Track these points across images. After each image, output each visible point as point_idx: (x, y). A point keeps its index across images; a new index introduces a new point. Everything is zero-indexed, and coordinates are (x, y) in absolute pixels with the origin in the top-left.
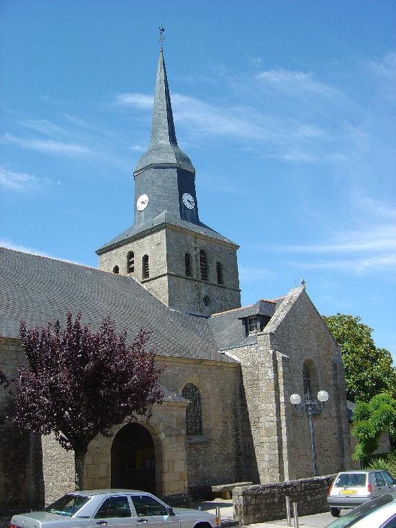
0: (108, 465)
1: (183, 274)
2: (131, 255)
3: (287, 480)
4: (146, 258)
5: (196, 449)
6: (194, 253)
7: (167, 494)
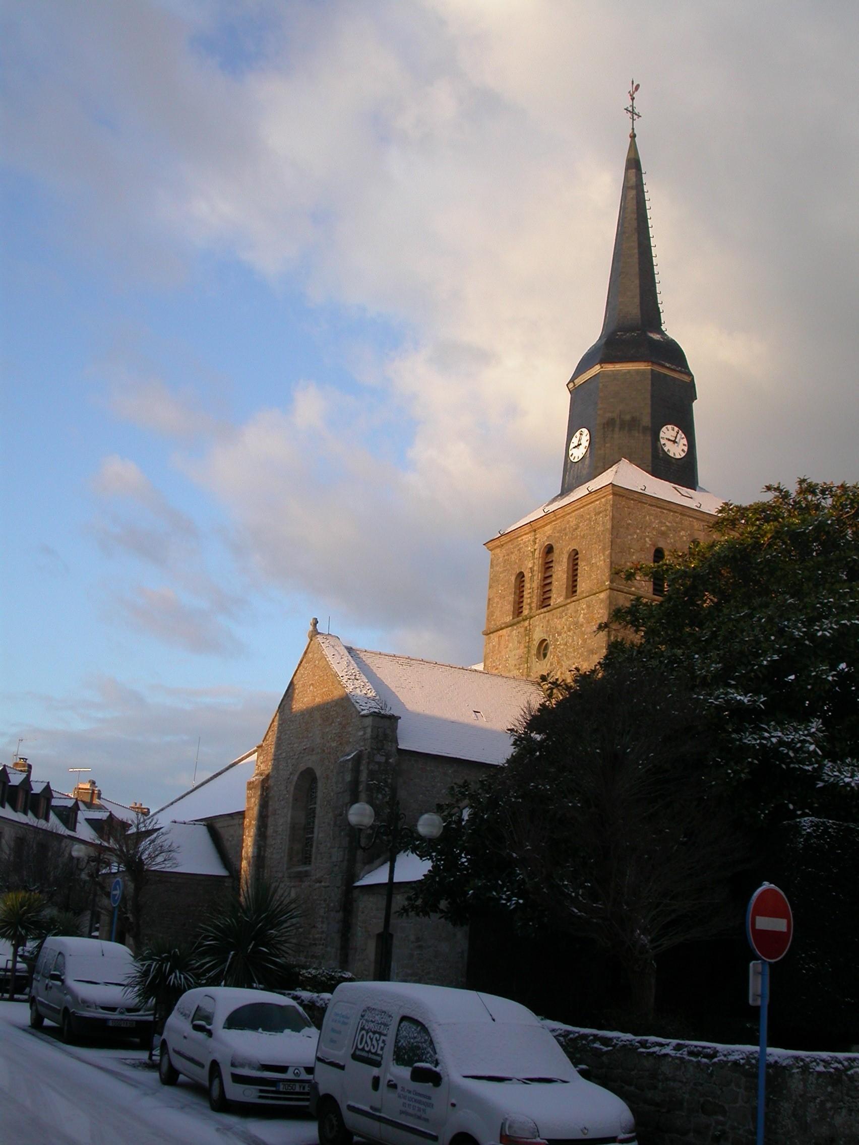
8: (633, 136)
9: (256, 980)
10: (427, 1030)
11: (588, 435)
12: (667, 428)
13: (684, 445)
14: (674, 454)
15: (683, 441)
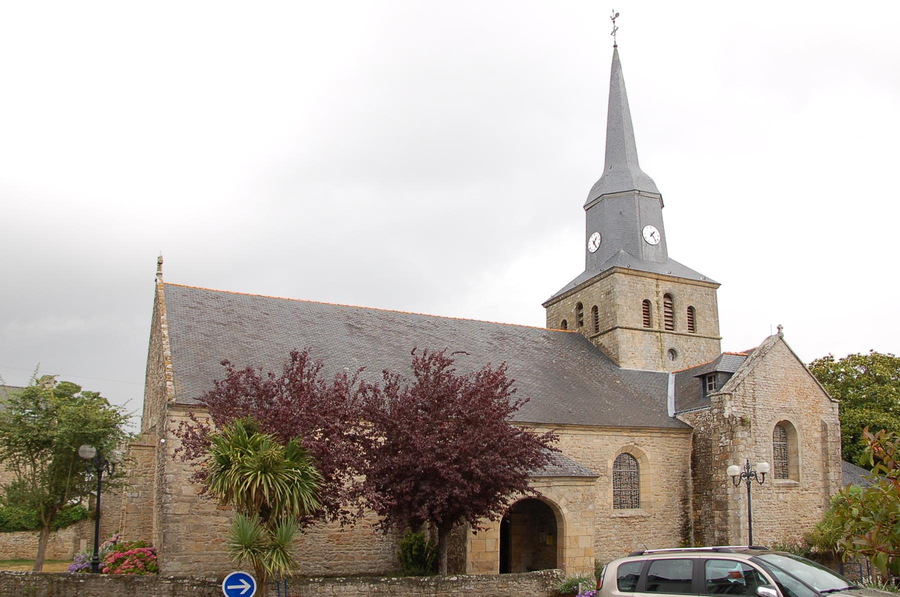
0: (497, 539)
1: (641, 326)
2: (580, 306)
4: (595, 309)
6: (655, 298)
7: (250, 586)
15: (657, 235)
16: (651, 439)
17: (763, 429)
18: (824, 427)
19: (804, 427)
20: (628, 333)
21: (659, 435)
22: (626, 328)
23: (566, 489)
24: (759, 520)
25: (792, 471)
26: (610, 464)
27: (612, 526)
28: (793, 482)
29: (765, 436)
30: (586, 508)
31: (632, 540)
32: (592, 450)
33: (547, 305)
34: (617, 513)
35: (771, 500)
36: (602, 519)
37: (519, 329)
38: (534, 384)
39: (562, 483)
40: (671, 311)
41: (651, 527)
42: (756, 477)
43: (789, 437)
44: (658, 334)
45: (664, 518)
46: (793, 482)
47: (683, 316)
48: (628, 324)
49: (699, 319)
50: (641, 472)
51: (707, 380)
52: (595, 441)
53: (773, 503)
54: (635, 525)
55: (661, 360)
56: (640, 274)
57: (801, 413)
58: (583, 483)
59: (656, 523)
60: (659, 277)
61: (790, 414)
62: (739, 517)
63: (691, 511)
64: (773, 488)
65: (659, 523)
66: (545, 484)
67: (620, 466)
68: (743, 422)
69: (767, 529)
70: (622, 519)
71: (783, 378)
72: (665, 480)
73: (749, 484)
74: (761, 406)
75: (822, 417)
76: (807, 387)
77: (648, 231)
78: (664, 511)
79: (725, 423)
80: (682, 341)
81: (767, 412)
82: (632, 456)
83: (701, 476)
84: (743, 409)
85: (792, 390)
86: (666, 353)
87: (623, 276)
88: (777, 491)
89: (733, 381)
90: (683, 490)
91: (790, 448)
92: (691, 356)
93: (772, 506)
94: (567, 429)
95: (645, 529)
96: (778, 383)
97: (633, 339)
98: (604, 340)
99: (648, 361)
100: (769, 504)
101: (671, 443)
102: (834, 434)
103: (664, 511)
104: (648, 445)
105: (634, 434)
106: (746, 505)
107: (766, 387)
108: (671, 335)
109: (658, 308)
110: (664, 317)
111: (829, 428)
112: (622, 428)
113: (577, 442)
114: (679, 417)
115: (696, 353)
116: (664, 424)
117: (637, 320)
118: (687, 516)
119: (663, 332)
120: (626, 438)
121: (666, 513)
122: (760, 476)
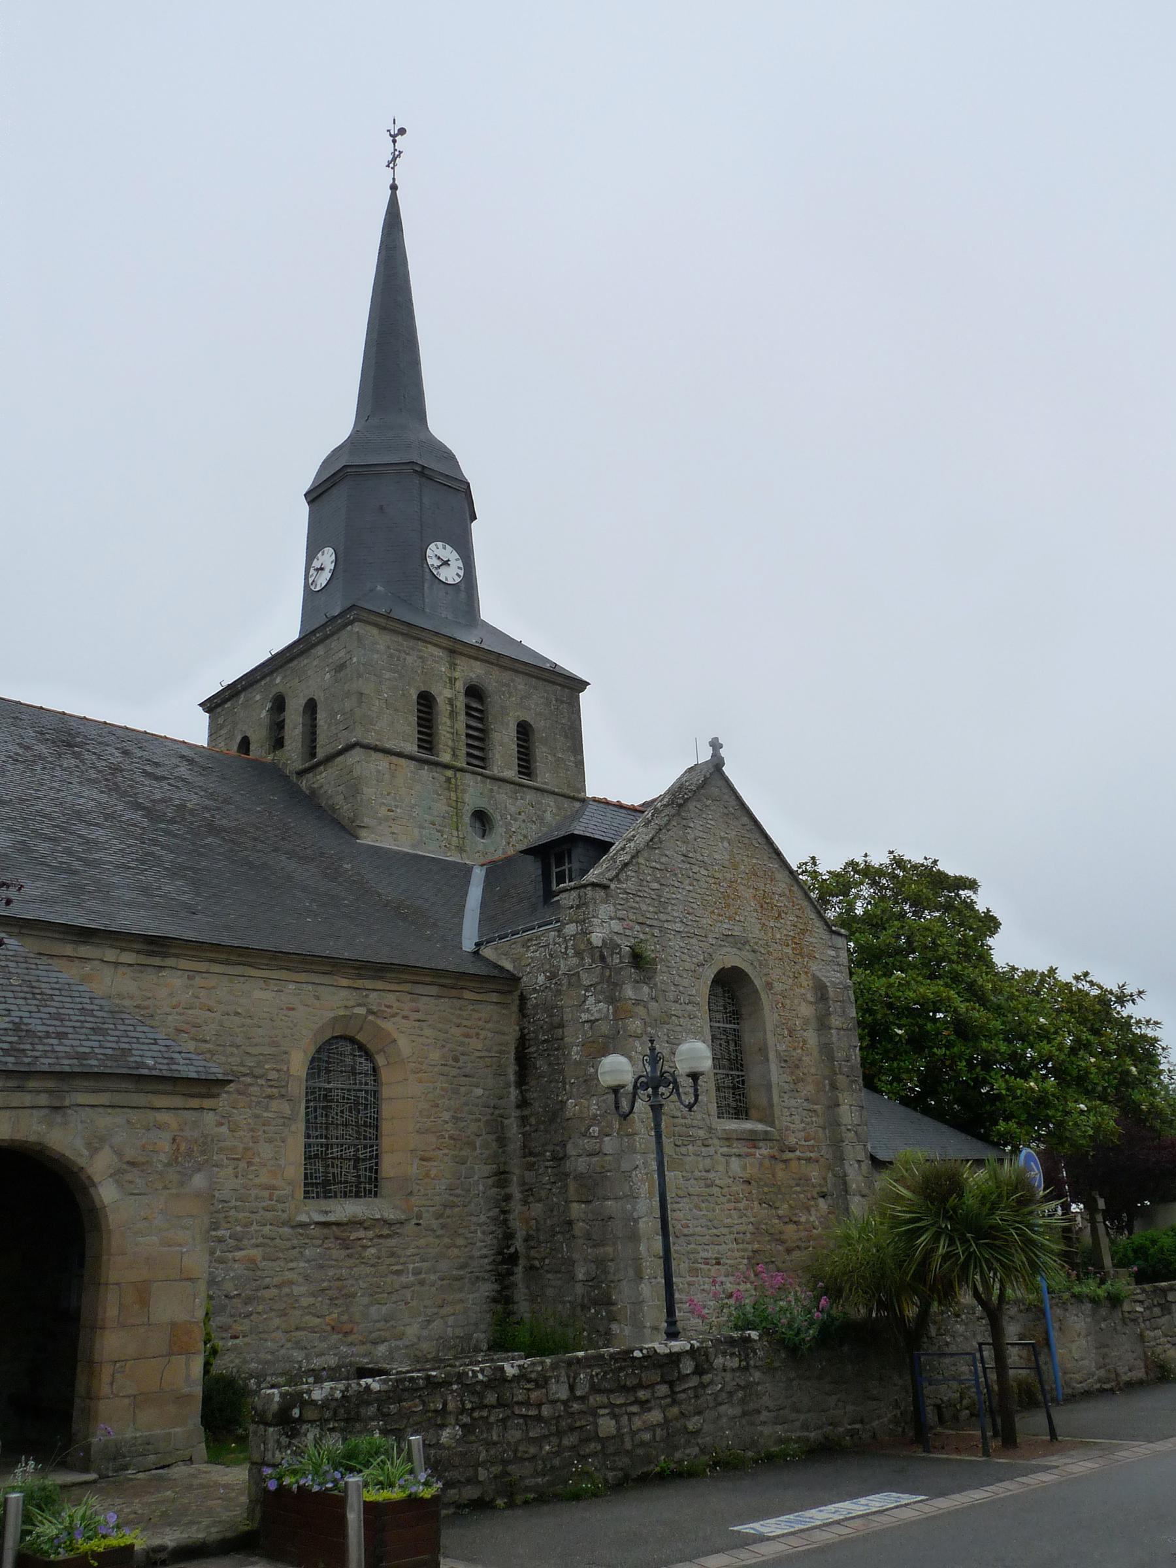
1: (411, 748)
2: (279, 704)
3: (1011, 1372)
4: (311, 707)
5: (345, 1244)
6: (448, 693)
8: (394, 187)
9: (1048, 1191)
10: (665, 1274)
11: (334, 555)
12: (436, 545)
13: (459, 568)
14: (446, 579)
15: (456, 564)
16: (412, 1001)
17: (686, 982)
18: (821, 991)
19: (778, 987)
20: (381, 763)
21: (434, 990)
22: (376, 749)
23: (117, 1119)
24: (686, 1231)
25: (756, 1097)
26: (298, 1064)
27: (295, 1252)
28: (760, 1127)
29: (690, 1003)
30: (182, 1184)
31: (354, 1295)
32: (248, 1021)
33: (212, 705)
34: (313, 1212)
35: (711, 1175)
36: (267, 1230)
37: (120, 733)
38: (115, 842)
39: (104, 1099)
40: (480, 726)
41: (410, 1252)
42: (676, 1087)
43: (744, 1011)
44: (450, 773)
45: (443, 1226)
46: (760, 1127)
47: (506, 740)
48: (380, 741)
49: (541, 752)
50: (385, 1092)
51: (553, 861)
52: (258, 994)
53: (718, 1182)
54: (365, 1247)
55: (455, 833)
56: (415, 632)
57: (769, 953)
58: (178, 1101)
59: (422, 1242)
60: (456, 650)
61: (744, 953)
62: (636, 1221)
63: (516, 1206)
64: (716, 1141)
65: (431, 1240)
66: (43, 1100)
67: (328, 1071)
68: (637, 959)
69: (705, 1255)
70: (326, 1231)
71: (727, 864)
72: (446, 1116)
73: (656, 1109)
74: (678, 926)
75: (814, 967)
76: (779, 891)
77: (437, 551)
78: (445, 1206)
79: (593, 961)
80: (503, 795)
81: (694, 941)
82: (361, 1047)
83: (537, 1107)
84: (637, 927)
85: (748, 894)
86: (467, 819)
87: (375, 631)
88: (725, 1150)
89: (612, 858)
90: (494, 1145)
91: (748, 1039)
92: (524, 832)
93: (715, 1190)
94: (177, 956)
95: (393, 1260)
96: (717, 875)
97: (393, 776)
98: (325, 779)
99: (425, 832)
100: (708, 1186)
101: (464, 1013)
102: (844, 1011)
103: (445, 1206)
104: (405, 1017)
105: (369, 984)
106: (651, 1186)
107: (687, 881)
108: (479, 778)
109: (453, 714)
110: (464, 737)
111: (831, 994)
112: (331, 965)
113: (203, 993)
114: (487, 952)
115: (534, 827)
116: (447, 963)
117: (405, 737)
118: (506, 1221)
119: (462, 770)
120: (344, 993)
121: (448, 1212)
122: (685, 1083)
